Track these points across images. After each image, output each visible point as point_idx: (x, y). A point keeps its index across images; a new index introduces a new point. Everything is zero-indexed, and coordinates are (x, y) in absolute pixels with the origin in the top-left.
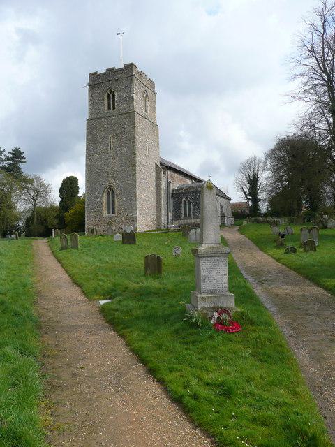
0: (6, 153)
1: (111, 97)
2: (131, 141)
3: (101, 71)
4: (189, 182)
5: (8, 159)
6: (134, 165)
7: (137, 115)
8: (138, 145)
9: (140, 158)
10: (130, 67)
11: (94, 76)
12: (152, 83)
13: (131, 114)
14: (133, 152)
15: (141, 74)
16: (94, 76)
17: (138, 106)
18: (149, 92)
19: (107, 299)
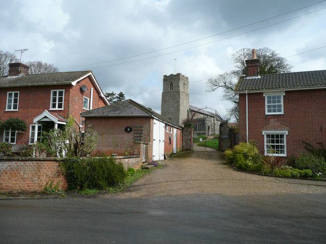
0: (117, 95)
1: (172, 85)
2: (178, 101)
3: (168, 75)
4: (202, 116)
5: (117, 97)
6: (179, 111)
7: (181, 92)
8: (181, 103)
9: (181, 108)
10: (179, 75)
11: (165, 76)
12: (187, 78)
13: (178, 92)
14: (179, 106)
15: (183, 76)
16: (165, 76)
17: (181, 89)
18: (186, 82)
19: (120, 201)
